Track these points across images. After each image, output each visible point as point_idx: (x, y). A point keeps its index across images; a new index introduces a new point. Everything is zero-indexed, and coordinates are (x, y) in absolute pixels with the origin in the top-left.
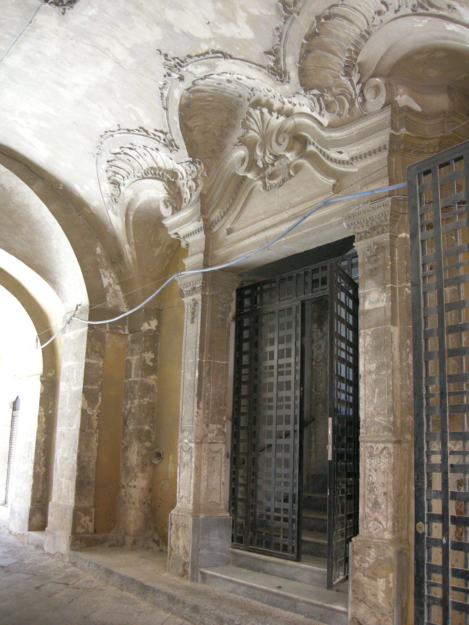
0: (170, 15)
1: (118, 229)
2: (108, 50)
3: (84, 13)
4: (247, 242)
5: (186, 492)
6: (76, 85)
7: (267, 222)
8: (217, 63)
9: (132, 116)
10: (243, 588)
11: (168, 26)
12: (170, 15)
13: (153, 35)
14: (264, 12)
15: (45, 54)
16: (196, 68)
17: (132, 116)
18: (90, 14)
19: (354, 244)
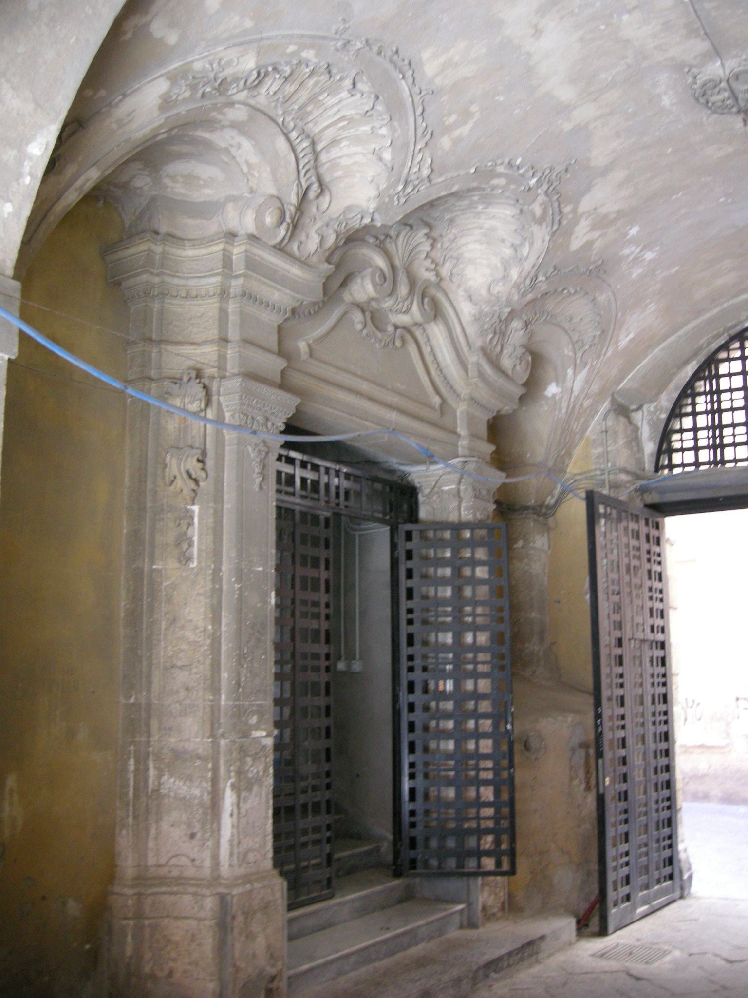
0: (619, 174)
1: (121, 124)
2: (595, 100)
3: (671, 92)
4: (342, 395)
5: (257, 839)
6: (538, 32)
7: (365, 386)
8: (544, 225)
9: (453, 118)
10: (353, 959)
11: (605, 172)
12: (619, 174)
13: (599, 156)
14: (595, 252)
15: (629, 12)
16: (541, 205)
17: (453, 118)
18: (664, 98)
19: (494, 507)
